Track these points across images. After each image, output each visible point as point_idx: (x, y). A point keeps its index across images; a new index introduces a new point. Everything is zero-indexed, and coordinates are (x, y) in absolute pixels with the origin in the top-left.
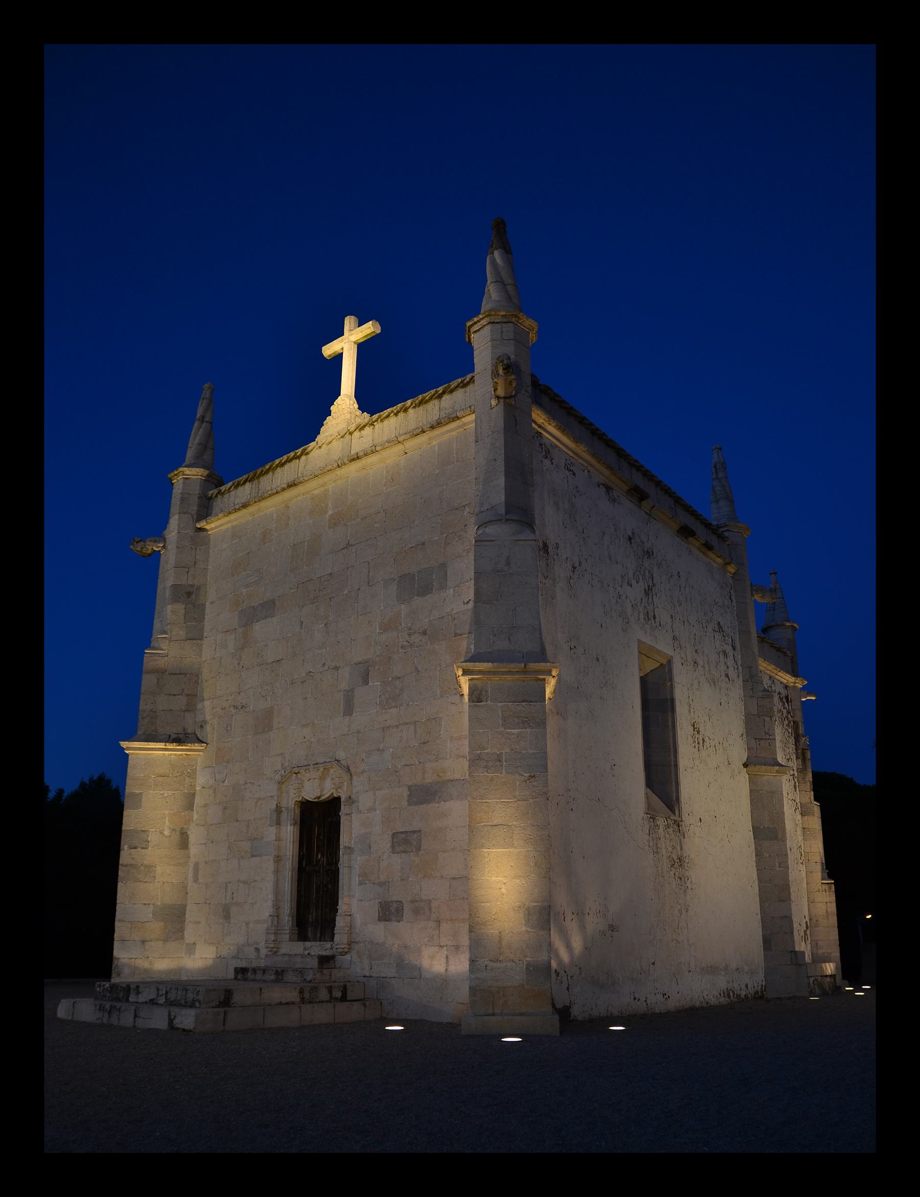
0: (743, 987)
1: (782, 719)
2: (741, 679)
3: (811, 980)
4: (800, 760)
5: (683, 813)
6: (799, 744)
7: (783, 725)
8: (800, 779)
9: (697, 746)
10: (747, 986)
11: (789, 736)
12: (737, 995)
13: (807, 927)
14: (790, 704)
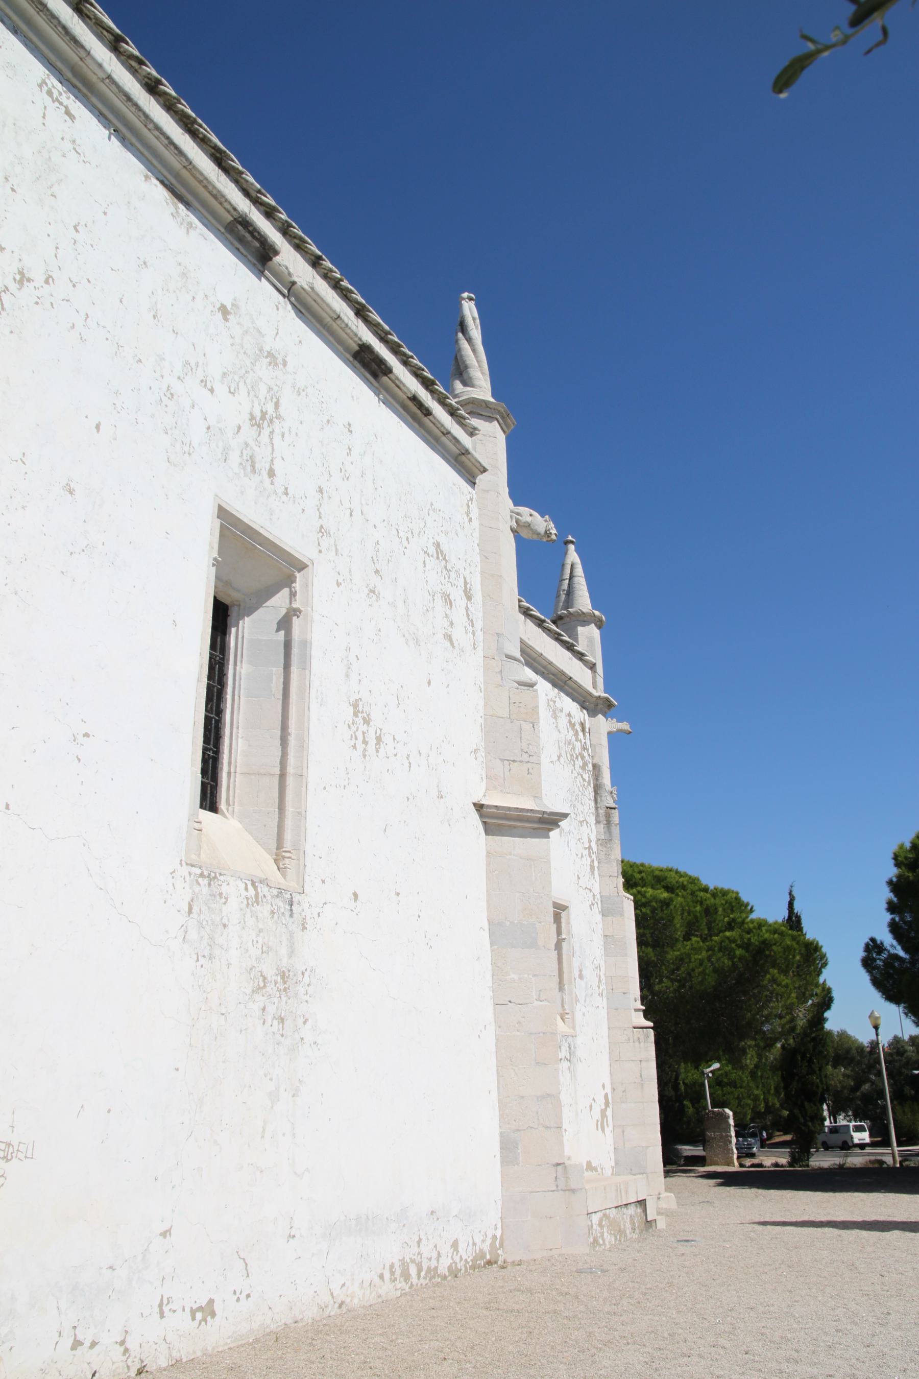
0: (446, 1249)
1: (572, 755)
2: (480, 652)
3: (595, 1218)
4: (602, 826)
5: (307, 878)
6: (601, 800)
7: (574, 765)
8: (602, 856)
9: (360, 747)
10: (455, 1245)
11: (584, 785)
12: (429, 1268)
13: (607, 1104)
14: (587, 735)
